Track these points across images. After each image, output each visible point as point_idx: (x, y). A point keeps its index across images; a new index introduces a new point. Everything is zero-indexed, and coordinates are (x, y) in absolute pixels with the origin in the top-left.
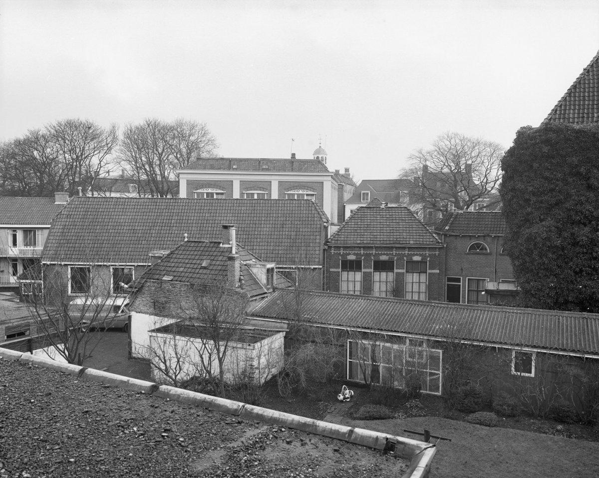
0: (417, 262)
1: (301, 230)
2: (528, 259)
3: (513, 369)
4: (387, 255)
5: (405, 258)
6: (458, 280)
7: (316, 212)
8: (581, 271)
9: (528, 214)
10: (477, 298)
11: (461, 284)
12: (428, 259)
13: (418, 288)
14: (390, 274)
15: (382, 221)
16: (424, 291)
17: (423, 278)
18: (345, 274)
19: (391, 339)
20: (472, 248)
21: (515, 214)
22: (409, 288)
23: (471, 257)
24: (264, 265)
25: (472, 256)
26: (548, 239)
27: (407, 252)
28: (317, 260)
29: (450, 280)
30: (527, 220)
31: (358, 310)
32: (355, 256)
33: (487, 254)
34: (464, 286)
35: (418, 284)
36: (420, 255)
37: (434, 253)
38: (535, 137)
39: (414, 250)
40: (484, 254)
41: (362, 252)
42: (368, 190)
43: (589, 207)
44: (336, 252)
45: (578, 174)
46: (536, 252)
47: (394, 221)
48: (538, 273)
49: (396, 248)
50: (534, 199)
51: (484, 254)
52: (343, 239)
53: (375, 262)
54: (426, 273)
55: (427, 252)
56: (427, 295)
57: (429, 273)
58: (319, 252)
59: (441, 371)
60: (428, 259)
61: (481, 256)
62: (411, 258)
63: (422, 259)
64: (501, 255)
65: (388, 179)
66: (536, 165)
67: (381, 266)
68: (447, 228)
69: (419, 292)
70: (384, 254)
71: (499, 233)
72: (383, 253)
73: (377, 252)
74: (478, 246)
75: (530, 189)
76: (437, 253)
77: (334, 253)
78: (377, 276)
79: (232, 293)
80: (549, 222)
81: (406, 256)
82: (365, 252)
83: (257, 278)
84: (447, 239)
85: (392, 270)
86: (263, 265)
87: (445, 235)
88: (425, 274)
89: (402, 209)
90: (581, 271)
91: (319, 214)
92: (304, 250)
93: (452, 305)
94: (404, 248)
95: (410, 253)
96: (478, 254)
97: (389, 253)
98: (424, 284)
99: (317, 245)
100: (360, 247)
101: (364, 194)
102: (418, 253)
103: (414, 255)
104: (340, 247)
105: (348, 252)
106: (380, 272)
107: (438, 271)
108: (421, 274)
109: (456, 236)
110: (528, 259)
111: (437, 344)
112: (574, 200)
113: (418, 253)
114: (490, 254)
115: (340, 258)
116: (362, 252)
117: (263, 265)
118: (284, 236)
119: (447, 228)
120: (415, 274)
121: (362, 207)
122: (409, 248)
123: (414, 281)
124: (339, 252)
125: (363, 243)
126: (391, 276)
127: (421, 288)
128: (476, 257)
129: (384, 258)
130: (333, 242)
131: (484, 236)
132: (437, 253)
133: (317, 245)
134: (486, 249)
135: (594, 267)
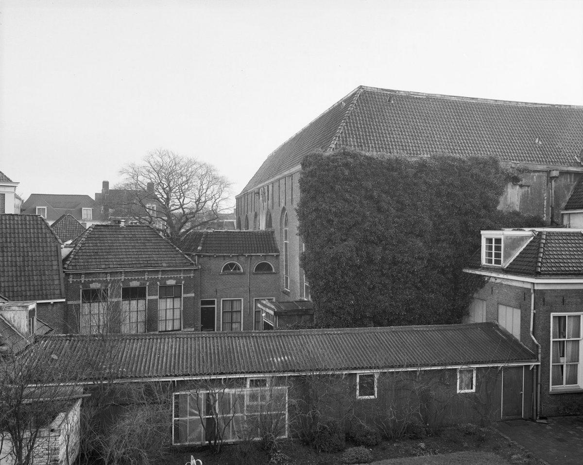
0: (171, 286)
1: (30, 254)
2: (331, 279)
3: (372, 397)
4: (138, 280)
5: (158, 283)
6: (213, 302)
7: (48, 231)
8: (374, 287)
9: (331, 234)
10: (231, 319)
11: (216, 306)
12: (183, 282)
13: (172, 314)
14: (177, 301)
15: (125, 241)
16: (178, 317)
17: (178, 303)
18: (86, 305)
19: (230, 384)
20: (226, 268)
21: (317, 234)
22: (162, 314)
23: (224, 277)
24: (26, 307)
25: (226, 276)
26: (350, 259)
27: (160, 276)
28: (57, 292)
29: (203, 303)
30: (329, 240)
31: (173, 352)
32: (100, 285)
33: (241, 274)
34: (219, 308)
35: (172, 310)
36: (174, 278)
37: (179, 276)
38: (336, 159)
39: (169, 273)
40: (238, 274)
41: (109, 278)
42: (44, 206)
43: (380, 228)
44: (75, 280)
45: (371, 197)
46: (339, 272)
47: (139, 241)
48: (339, 292)
49: (148, 271)
50: (336, 220)
51: (238, 274)
52: (82, 264)
53: (84, 291)
54: (181, 297)
55: (182, 275)
56: (182, 322)
57: (184, 298)
58: (60, 282)
59: (287, 410)
60: (183, 282)
61: (235, 276)
62: (165, 283)
63: (176, 283)
64: (254, 274)
65: (36, 193)
66: (337, 187)
67: (131, 294)
68: (199, 248)
69: (173, 320)
70: (135, 280)
71: (252, 253)
72: (169, 276)
73: (126, 278)
74: (232, 265)
75: (334, 209)
76: (192, 275)
77: (111, 279)
78: (125, 305)
79: (11, 349)
80: (351, 242)
81: (159, 281)
82: (150, 277)
83: (13, 326)
84: (201, 260)
85: (105, 299)
86: (23, 306)
87: (199, 256)
88: (179, 299)
89: (145, 228)
90: (374, 287)
91: (52, 233)
92: (37, 280)
93: (205, 333)
94: (158, 271)
95: (163, 277)
96: (232, 274)
97: (140, 278)
98: (178, 310)
99: (54, 272)
100: (107, 273)
101: (38, 209)
102: (172, 276)
103: (168, 279)
104: (81, 274)
105: (90, 279)
106: (138, 300)
107: (193, 295)
108: (176, 300)
109: (210, 256)
110: (331, 279)
111: (280, 381)
112: (369, 221)
113: (172, 276)
114: (244, 273)
115: (81, 287)
116: (109, 278)
117: (23, 306)
118: (6, 263)
119: (199, 248)
120: (168, 300)
121: (97, 225)
122: (163, 271)
123: (168, 308)
124: (79, 280)
125: (109, 268)
126: (141, 304)
127: (175, 315)
128: (231, 277)
129: (135, 284)
130: (71, 267)
131: (238, 256)
132: (192, 275)
133: (54, 272)
134: (239, 269)
135: (384, 283)
